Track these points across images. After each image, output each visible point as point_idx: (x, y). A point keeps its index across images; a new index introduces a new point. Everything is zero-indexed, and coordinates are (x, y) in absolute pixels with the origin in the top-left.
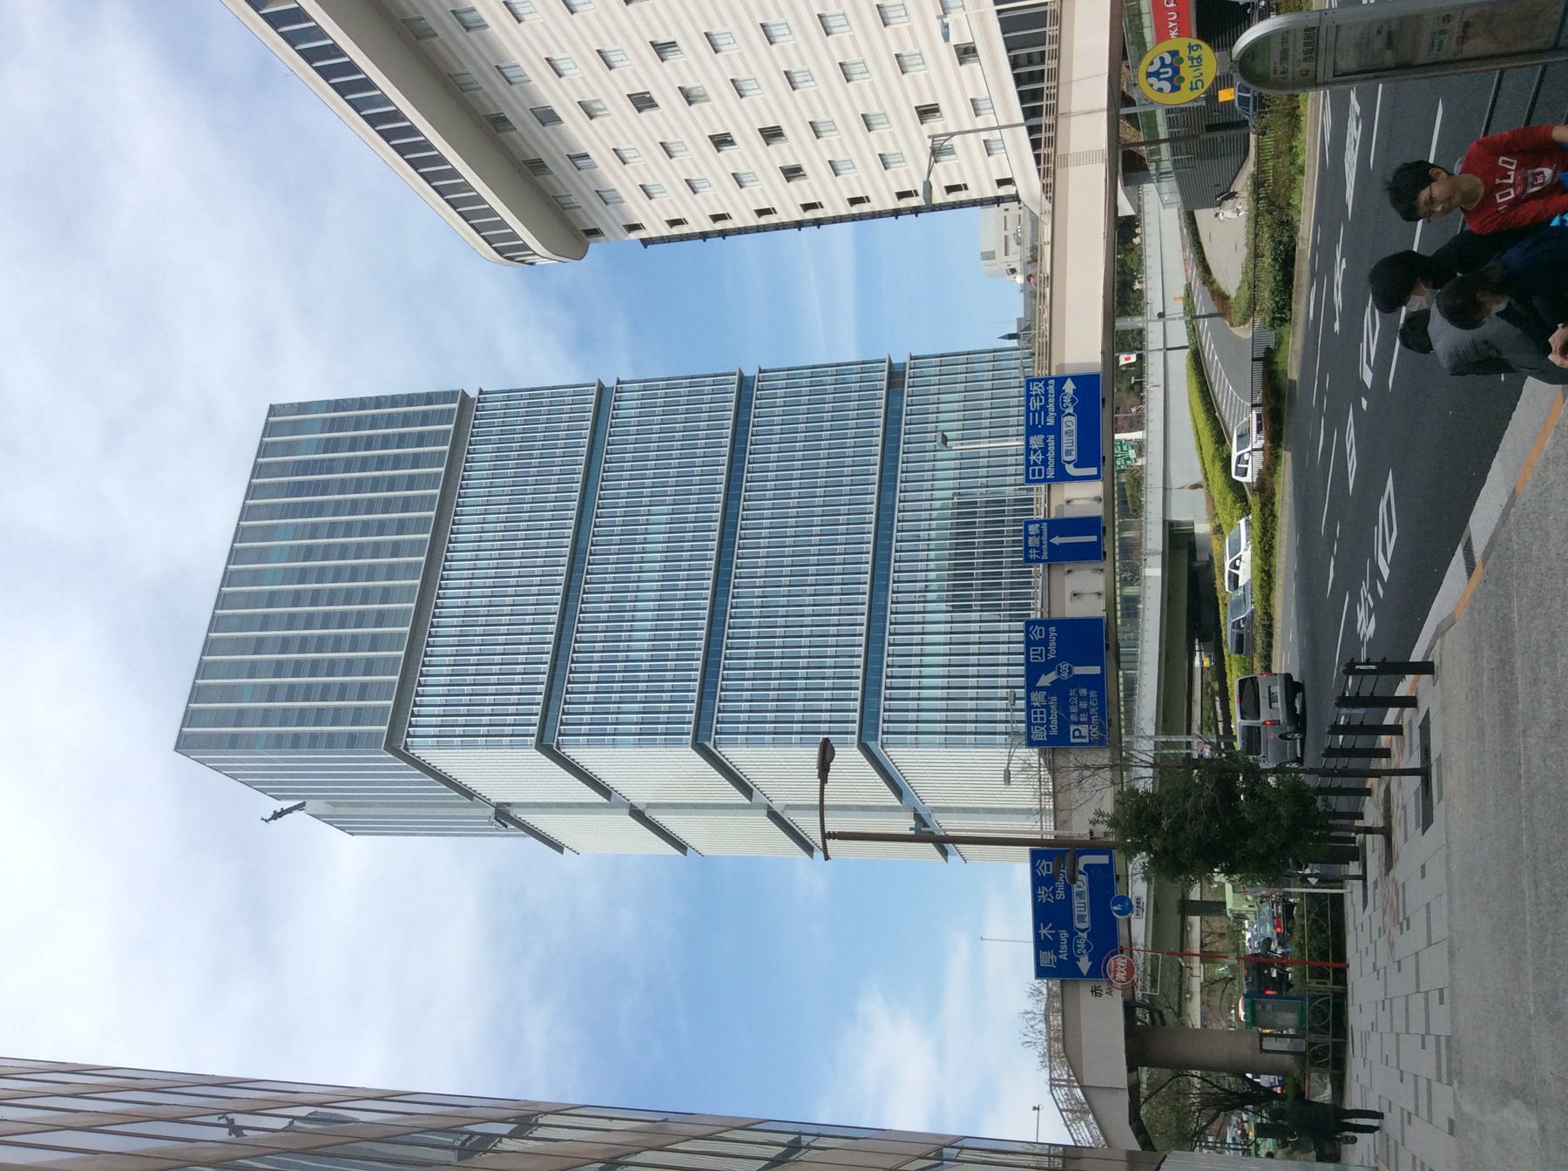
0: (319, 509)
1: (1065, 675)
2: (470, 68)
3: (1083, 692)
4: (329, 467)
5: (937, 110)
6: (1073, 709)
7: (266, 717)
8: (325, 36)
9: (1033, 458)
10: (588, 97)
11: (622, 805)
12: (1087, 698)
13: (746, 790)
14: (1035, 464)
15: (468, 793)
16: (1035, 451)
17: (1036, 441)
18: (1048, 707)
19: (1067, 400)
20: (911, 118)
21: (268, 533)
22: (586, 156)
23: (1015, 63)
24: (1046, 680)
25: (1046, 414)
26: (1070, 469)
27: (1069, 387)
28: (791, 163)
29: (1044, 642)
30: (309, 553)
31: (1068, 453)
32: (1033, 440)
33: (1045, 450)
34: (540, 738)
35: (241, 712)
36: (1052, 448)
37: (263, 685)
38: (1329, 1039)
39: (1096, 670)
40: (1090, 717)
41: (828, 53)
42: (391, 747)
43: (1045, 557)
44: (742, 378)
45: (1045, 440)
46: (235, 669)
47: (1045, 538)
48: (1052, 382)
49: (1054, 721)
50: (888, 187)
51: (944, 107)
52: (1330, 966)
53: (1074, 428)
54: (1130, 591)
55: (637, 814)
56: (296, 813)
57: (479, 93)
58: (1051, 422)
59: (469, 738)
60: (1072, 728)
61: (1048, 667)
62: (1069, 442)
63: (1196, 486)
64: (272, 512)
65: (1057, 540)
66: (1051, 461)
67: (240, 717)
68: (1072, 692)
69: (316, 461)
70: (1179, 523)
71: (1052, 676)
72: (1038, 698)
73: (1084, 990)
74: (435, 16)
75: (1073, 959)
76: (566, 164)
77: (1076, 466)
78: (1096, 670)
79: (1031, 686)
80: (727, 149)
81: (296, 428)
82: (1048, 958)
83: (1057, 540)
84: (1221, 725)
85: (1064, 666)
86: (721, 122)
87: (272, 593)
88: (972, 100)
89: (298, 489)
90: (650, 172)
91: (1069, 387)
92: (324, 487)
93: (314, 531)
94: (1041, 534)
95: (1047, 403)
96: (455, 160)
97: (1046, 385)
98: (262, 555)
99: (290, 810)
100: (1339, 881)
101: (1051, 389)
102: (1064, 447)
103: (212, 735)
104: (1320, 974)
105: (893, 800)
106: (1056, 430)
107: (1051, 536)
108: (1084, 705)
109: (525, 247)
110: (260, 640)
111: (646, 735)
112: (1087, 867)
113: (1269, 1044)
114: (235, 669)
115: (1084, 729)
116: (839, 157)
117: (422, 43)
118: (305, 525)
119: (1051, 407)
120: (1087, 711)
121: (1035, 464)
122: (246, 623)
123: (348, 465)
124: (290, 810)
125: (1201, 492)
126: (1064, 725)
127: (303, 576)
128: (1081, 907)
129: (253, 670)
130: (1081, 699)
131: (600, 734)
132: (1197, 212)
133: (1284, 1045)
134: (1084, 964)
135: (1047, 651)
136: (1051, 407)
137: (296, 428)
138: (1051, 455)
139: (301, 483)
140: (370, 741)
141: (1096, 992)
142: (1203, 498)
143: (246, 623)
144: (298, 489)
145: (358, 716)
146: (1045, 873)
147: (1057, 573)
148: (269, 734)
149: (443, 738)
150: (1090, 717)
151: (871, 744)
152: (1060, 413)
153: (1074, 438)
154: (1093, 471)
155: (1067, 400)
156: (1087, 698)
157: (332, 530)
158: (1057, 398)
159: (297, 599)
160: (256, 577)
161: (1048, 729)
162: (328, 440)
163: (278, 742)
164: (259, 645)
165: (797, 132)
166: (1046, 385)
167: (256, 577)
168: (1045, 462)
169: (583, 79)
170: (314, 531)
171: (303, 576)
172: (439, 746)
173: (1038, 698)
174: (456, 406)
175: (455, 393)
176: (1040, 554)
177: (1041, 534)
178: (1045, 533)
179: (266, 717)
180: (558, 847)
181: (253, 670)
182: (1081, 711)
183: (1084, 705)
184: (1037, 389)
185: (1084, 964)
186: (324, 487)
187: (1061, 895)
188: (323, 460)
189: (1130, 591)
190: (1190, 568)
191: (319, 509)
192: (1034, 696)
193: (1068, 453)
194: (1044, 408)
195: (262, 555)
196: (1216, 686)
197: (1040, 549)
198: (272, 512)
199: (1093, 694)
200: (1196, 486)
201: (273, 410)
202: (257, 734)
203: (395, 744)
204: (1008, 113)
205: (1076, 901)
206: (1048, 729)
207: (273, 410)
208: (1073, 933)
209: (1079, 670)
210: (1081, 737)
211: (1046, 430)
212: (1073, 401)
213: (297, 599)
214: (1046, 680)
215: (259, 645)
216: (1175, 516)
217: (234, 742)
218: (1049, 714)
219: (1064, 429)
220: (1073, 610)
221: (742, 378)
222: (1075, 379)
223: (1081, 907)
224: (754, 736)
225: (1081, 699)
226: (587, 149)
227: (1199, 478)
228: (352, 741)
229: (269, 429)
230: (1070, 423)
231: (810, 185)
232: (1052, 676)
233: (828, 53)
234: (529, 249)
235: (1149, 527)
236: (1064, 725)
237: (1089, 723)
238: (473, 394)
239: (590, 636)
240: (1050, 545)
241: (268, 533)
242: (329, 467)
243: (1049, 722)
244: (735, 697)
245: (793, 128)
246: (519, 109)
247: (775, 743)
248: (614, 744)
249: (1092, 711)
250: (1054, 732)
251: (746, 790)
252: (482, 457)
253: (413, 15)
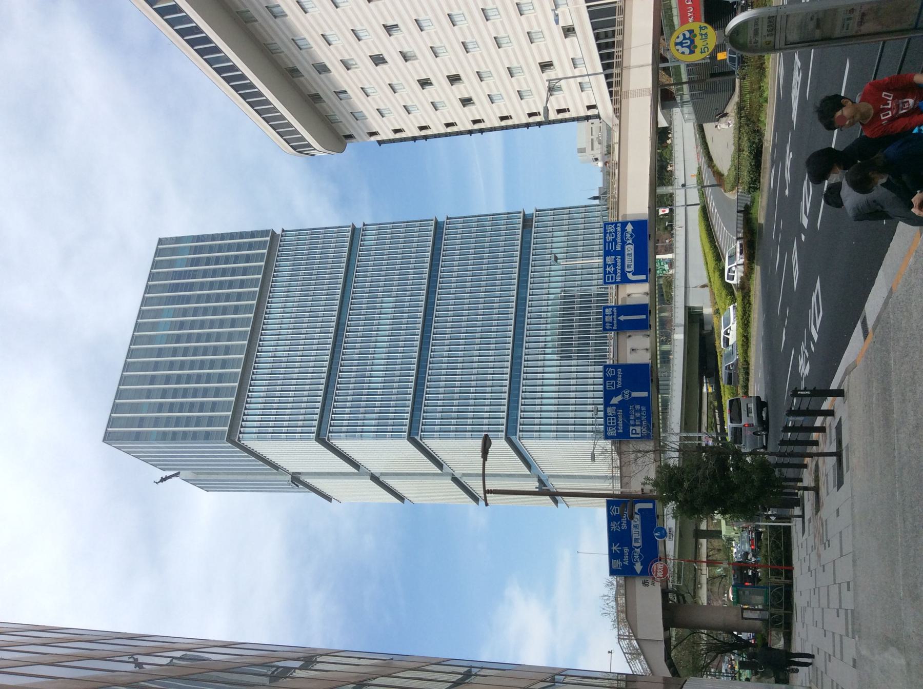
0: (188, 300)
1: (627, 397)
2: (277, 40)
3: (638, 407)
4: (194, 275)
5: (552, 65)
6: (632, 417)
7: (157, 422)
8: (191, 21)
9: (608, 269)
10: (346, 57)
11: (366, 474)
12: (640, 411)
13: (439, 465)
14: (609, 273)
15: (275, 467)
16: (609, 265)
17: (610, 260)
18: (617, 416)
19: (628, 235)
20: (536, 69)
21: (158, 313)
22: (345, 92)
23: (597, 37)
24: (615, 400)
25: (616, 244)
26: (630, 276)
27: (629, 228)
28: (466, 96)
29: (615, 378)
30: (182, 325)
31: (629, 266)
32: (608, 259)
33: (615, 265)
34: (318, 434)
35: (142, 419)
36: (619, 263)
37: (155, 403)
38: (782, 612)
39: (645, 394)
40: (641, 422)
41: (487, 31)
42: (230, 439)
43: (615, 328)
44: (437, 222)
45: (615, 259)
46: (138, 394)
47: (615, 317)
48: (619, 225)
49: (621, 424)
50: (523, 110)
51: (555, 63)
52: (783, 569)
53: (632, 252)
54: (665, 347)
55: (375, 479)
56: (174, 478)
57: (282, 55)
58: (619, 248)
59: (276, 434)
60: (631, 428)
61: (617, 392)
62: (630, 260)
63: (704, 286)
64: (160, 301)
65: (622, 318)
66: (619, 271)
67: (141, 422)
68: (631, 407)
69: (186, 271)
70: (694, 308)
71: (620, 398)
72: (611, 411)
73: (638, 582)
74: (283, 42)
75: (631, 564)
76: (334, 97)
77: (634, 274)
78: (645, 394)
79: (607, 404)
80: (428, 88)
81: (174, 252)
82: (617, 563)
83: (622, 318)
84: (718, 427)
85: (627, 392)
86: (425, 72)
87: (160, 349)
88: (572, 59)
89: (176, 288)
90: (383, 101)
91: (629, 228)
92: (191, 287)
93: (185, 313)
94: (613, 314)
95: (616, 237)
96: (268, 94)
97: (616, 227)
98: (154, 327)
99: (171, 477)
100: (788, 519)
101: (619, 229)
102: (627, 263)
103: (124, 432)
104: (777, 573)
105: (526, 471)
106: (622, 253)
107: (618, 315)
108: (638, 415)
109: (309, 145)
110: (153, 377)
111: (380, 432)
112: (640, 510)
113: (747, 614)
114: (138, 394)
115: (638, 429)
116: (494, 92)
117: (249, 25)
118: (180, 309)
119: (619, 240)
120: (640, 418)
121: (609, 273)
122: (145, 366)
123: (205, 274)
124: (171, 477)
125: (707, 290)
126: (626, 426)
127: (178, 339)
128: (636, 534)
129: (149, 394)
130: (636, 411)
131: (354, 432)
132: (704, 125)
133: (756, 615)
134: (638, 567)
135: (616, 383)
136: (619, 240)
137: (174, 252)
138: (619, 268)
139: (178, 284)
140: (218, 436)
141: (645, 583)
142: (708, 293)
143: (145, 366)
144: (176, 288)
145: (211, 421)
146: (615, 514)
147: (622, 337)
148: (158, 432)
149: (260, 434)
150: (641, 422)
151: (513, 438)
152: (624, 243)
153: (632, 258)
154: (643, 277)
155: (628, 235)
156: (640, 411)
157: (196, 312)
158: (622, 234)
159: (175, 352)
160: (151, 340)
161: (617, 429)
162: (193, 259)
163: (164, 436)
164: (153, 380)
165: (469, 78)
166: (616, 227)
167: (151, 340)
168: (615, 272)
169: (343, 46)
170: (185, 313)
171: (178, 339)
172: (258, 439)
173: (611, 411)
174: (268, 239)
175: (267, 231)
176: (612, 326)
177: (613, 314)
178: (615, 313)
179: (157, 422)
180: (329, 498)
181: (149, 394)
182: (636, 418)
183: (638, 415)
184: (610, 229)
185: (638, 567)
186: (191, 287)
187: (624, 527)
188: (190, 271)
189: (665, 347)
190: (700, 335)
191: (188, 300)
192: (609, 409)
193: (629, 266)
194: (615, 240)
195: (154, 327)
196: (716, 404)
197: (612, 323)
198: (160, 301)
199: (643, 408)
200: (704, 286)
201: (161, 241)
202: (151, 432)
203: (232, 438)
204: (593, 66)
205: (633, 530)
206: (617, 429)
207: (161, 241)
208: (631, 549)
209: (635, 394)
210: (636, 433)
211: (616, 253)
212: (632, 236)
213: (175, 352)
214: (615, 400)
215: (153, 380)
216: (692, 304)
217: (138, 437)
218: (617, 420)
219: (627, 252)
220: (632, 359)
221: (437, 222)
222: (633, 223)
223: (636, 534)
224: (444, 433)
225: (636, 411)
226: (346, 88)
227: (706, 281)
228: (207, 436)
229: (158, 253)
230: (630, 249)
231: (477, 109)
232: (620, 398)
233: (487, 31)
234: (311, 146)
235: (677, 310)
236: (626, 426)
237: (641, 425)
238: (278, 232)
239: (348, 374)
240: (618, 321)
241: (158, 313)
242: (194, 275)
243: (617, 425)
244: (433, 410)
245: (467, 75)
246: (305, 64)
247: (456, 437)
248: (361, 438)
249: (643, 418)
250: (621, 431)
251: (439, 465)
252: (284, 269)
253: (243, 9)
